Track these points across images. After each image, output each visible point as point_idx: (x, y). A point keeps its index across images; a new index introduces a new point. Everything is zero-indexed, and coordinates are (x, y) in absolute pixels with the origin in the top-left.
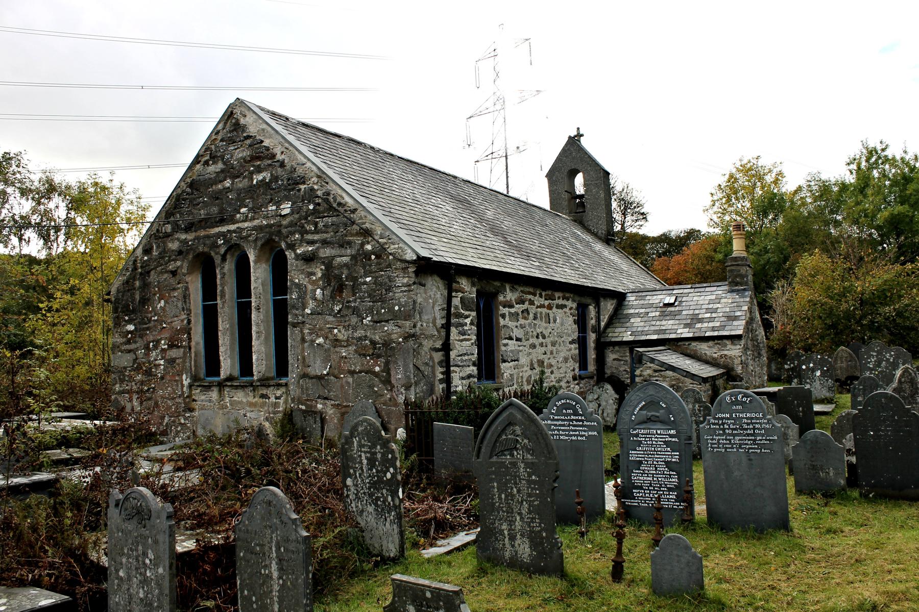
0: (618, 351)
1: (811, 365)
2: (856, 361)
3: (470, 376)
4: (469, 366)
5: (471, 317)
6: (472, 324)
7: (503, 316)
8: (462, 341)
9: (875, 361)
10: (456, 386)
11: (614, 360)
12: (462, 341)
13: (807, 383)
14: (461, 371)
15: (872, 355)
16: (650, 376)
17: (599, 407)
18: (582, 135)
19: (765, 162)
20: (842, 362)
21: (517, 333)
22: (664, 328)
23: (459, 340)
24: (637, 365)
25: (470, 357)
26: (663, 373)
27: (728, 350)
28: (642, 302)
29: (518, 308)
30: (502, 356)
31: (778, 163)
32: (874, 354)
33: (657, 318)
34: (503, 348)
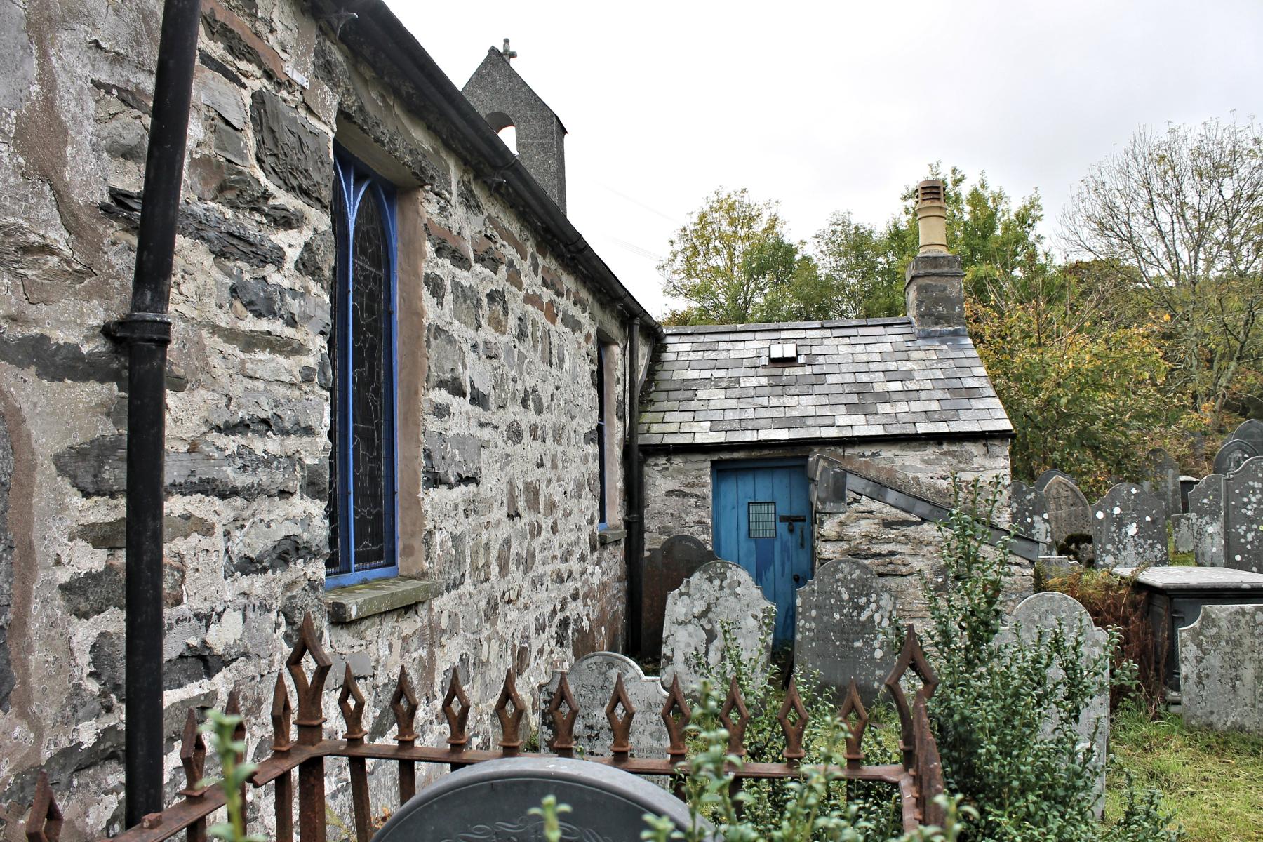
0: (680, 471)
1: (1117, 511)
2: (1084, 505)
3: (288, 552)
4: (284, 494)
5: (306, 234)
6: (307, 266)
7: (436, 286)
8: (251, 342)
9: (1259, 502)
10: (206, 619)
11: (670, 493)
12: (251, 342)
13: (1108, 552)
14: (239, 523)
15: (1254, 489)
16: (870, 538)
17: (709, 641)
18: (513, 55)
19: (755, 199)
20: (1059, 507)
21: (475, 372)
22: (795, 413)
23: (231, 336)
24: (829, 507)
25: (293, 443)
26: (911, 531)
27: (977, 470)
28: (712, 355)
29: (477, 278)
30: (428, 456)
31: (773, 201)
32: (1257, 485)
33: (767, 390)
34: (433, 424)
